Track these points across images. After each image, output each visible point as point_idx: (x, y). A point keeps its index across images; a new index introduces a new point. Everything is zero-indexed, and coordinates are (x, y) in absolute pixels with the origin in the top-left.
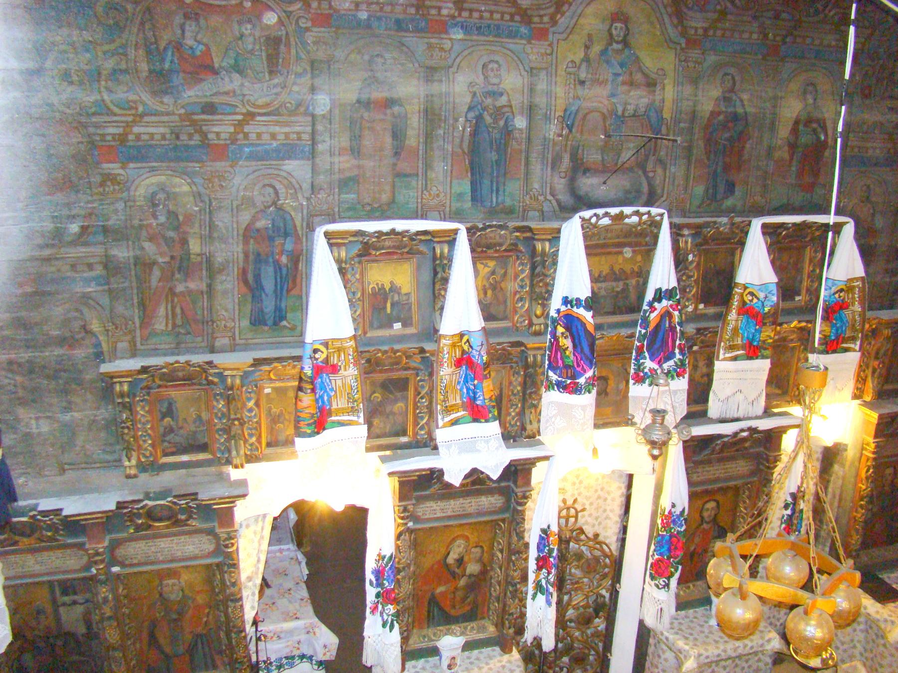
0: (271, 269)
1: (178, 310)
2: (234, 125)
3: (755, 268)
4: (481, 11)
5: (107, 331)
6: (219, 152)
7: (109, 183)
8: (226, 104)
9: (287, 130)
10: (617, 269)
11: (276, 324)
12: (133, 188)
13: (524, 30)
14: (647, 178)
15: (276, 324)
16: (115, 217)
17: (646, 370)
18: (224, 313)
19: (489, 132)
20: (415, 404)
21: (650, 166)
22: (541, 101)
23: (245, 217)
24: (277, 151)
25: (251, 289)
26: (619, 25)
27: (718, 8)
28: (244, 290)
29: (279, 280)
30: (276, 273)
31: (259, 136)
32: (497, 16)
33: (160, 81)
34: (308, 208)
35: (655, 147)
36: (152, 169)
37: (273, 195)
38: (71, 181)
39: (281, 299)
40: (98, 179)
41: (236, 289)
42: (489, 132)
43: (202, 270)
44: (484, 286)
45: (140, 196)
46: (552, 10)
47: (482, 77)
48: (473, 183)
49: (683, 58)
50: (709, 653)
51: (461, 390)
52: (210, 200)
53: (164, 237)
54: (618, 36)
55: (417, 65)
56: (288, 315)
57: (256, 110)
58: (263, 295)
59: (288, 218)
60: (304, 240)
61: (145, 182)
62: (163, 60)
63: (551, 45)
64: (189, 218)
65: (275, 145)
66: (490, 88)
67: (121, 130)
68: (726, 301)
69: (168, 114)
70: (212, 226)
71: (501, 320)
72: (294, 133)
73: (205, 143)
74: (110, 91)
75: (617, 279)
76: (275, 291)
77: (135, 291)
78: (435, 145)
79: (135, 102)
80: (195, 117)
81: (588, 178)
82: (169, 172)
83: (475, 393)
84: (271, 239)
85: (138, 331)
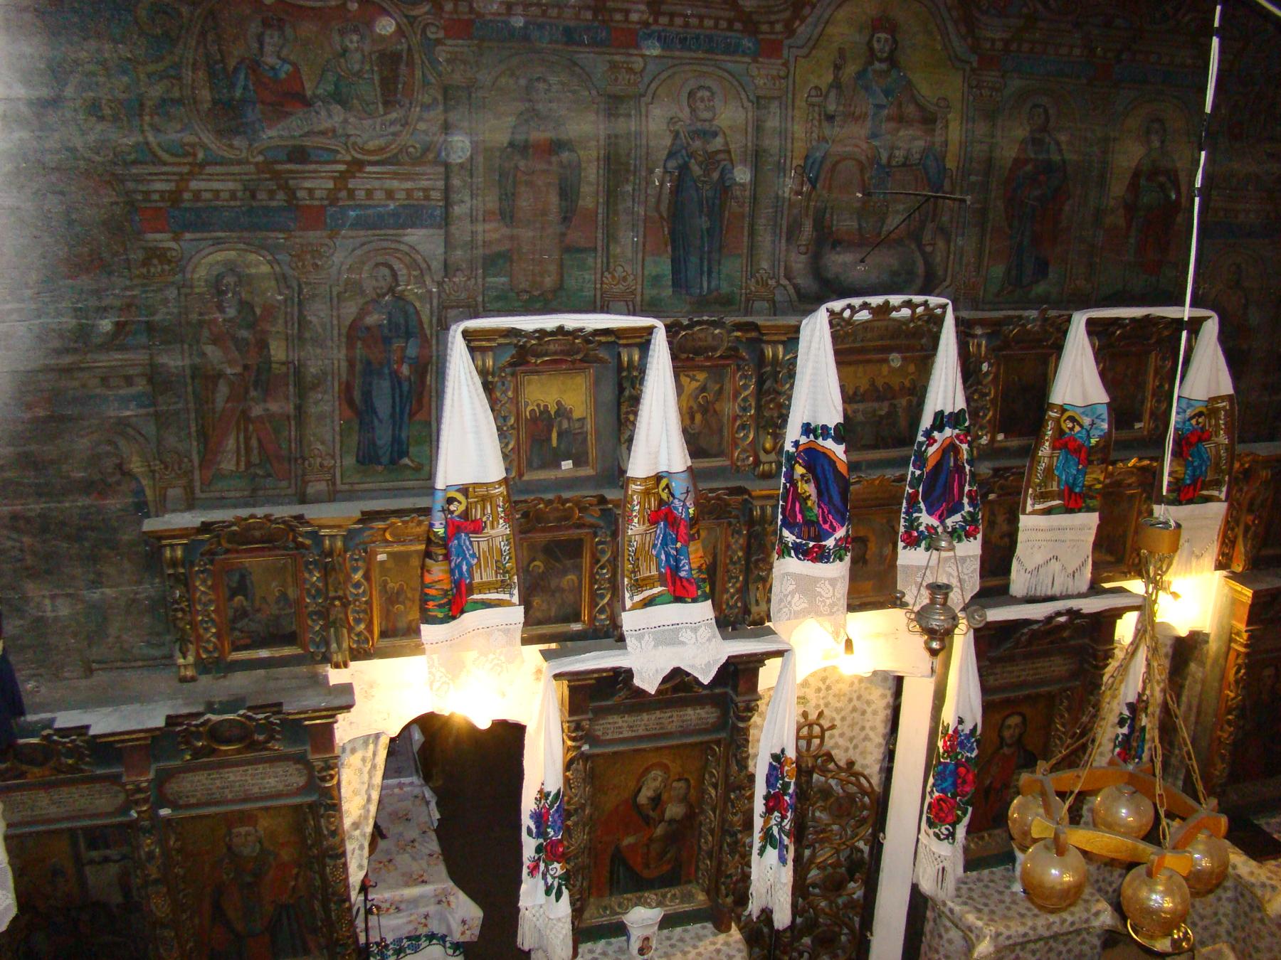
0: (386, 384)
1: (254, 443)
2: (334, 178)
3: (1078, 381)
4: (686, 16)
5: (153, 472)
6: (313, 216)
7: (155, 261)
8: (322, 148)
9: (409, 185)
10: (880, 383)
11: (393, 461)
12: (189, 268)
13: (747, 43)
14: (923, 253)
15: (393, 461)
16: (165, 310)
17: (922, 528)
18: (320, 447)
19: (697, 189)
20: (592, 576)
21: (927, 238)
22: (772, 143)
23: (350, 310)
24: (395, 214)
25: (358, 413)
26: (883, 36)
27: (1025, 11)
28: (348, 413)
29: (397, 400)
30: (393, 389)
31: (370, 193)
32: (709, 23)
33: (228, 116)
34: (439, 297)
35: (935, 210)
36: (217, 242)
37: (389, 279)
38: (101, 259)
39: (400, 428)
40: (140, 255)
41: (337, 412)
42: (697, 189)
43: (288, 385)
44: (691, 408)
45: (199, 279)
46: (787, 14)
47: (687, 110)
48: (675, 261)
49: (974, 83)
50: (1012, 932)
51: (658, 556)
52: (299, 286)
53: (234, 338)
54: (882, 51)
55: (594, 92)
56: (411, 449)
57: (366, 158)
58: (376, 422)
59: (412, 310)
60: (434, 342)
61: (208, 260)
62: (232, 86)
63: (785, 64)
64: (269, 311)
65: (392, 207)
66: (699, 125)
67: (172, 186)
68: (1036, 430)
69: (239, 163)
70: (302, 323)
71: (715, 456)
72: (419, 189)
73: (292, 204)
74: (157, 129)
75: (880, 398)
76: (393, 415)
77: (193, 415)
78: (621, 207)
79: (193, 145)
80: (279, 167)
81: (839, 253)
82: (242, 246)
83: (677, 561)
84: (387, 341)
85: (197, 473)
